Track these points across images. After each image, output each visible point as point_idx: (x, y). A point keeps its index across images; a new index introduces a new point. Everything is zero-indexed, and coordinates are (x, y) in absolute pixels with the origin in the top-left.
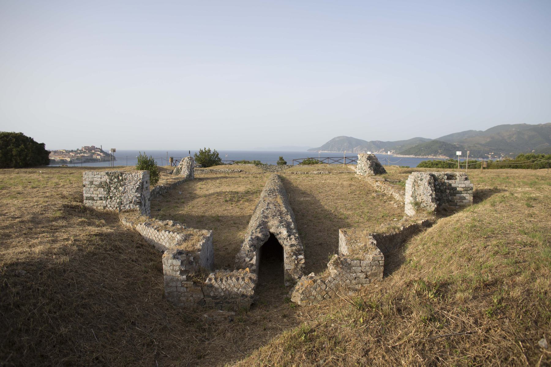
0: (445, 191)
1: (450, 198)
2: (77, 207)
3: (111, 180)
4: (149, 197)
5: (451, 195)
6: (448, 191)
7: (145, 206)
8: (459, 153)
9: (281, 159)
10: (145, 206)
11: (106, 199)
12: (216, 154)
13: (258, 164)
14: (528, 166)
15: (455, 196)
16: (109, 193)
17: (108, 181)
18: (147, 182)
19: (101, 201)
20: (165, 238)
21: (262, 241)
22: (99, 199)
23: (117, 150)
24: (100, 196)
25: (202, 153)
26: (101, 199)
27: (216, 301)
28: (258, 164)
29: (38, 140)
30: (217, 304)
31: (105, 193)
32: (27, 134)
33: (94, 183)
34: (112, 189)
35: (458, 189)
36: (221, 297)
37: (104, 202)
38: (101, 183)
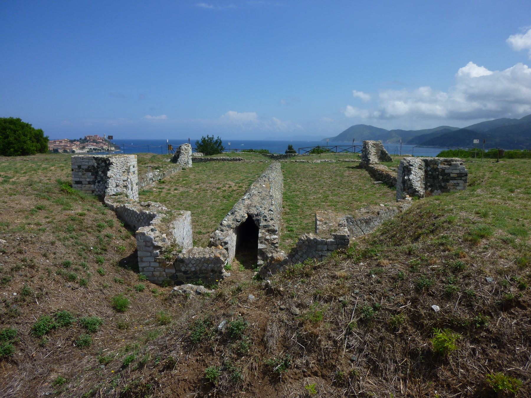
0: (438, 177)
1: (443, 184)
2: (260, 273)
3: (98, 164)
4: (136, 181)
5: (443, 182)
6: (441, 177)
7: (132, 190)
8: (476, 141)
9: (290, 148)
10: (132, 190)
11: (94, 183)
12: (219, 143)
13: (264, 153)
14: (523, 153)
15: (448, 182)
16: (96, 178)
17: (96, 165)
18: (134, 167)
19: (89, 185)
20: (144, 218)
21: (239, 222)
22: (87, 183)
23: (114, 138)
24: (88, 180)
25: (204, 140)
26: (89, 183)
27: (187, 276)
28: (264, 153)
29: (36, 126)
30: (187, 278)
31: (94, 177)
32: (25, 120)
33: (82, 167)
34: (100, 173)
35: (452, 175)
36: (191, 272)
37: (92, 186)
38: (89, 167)
